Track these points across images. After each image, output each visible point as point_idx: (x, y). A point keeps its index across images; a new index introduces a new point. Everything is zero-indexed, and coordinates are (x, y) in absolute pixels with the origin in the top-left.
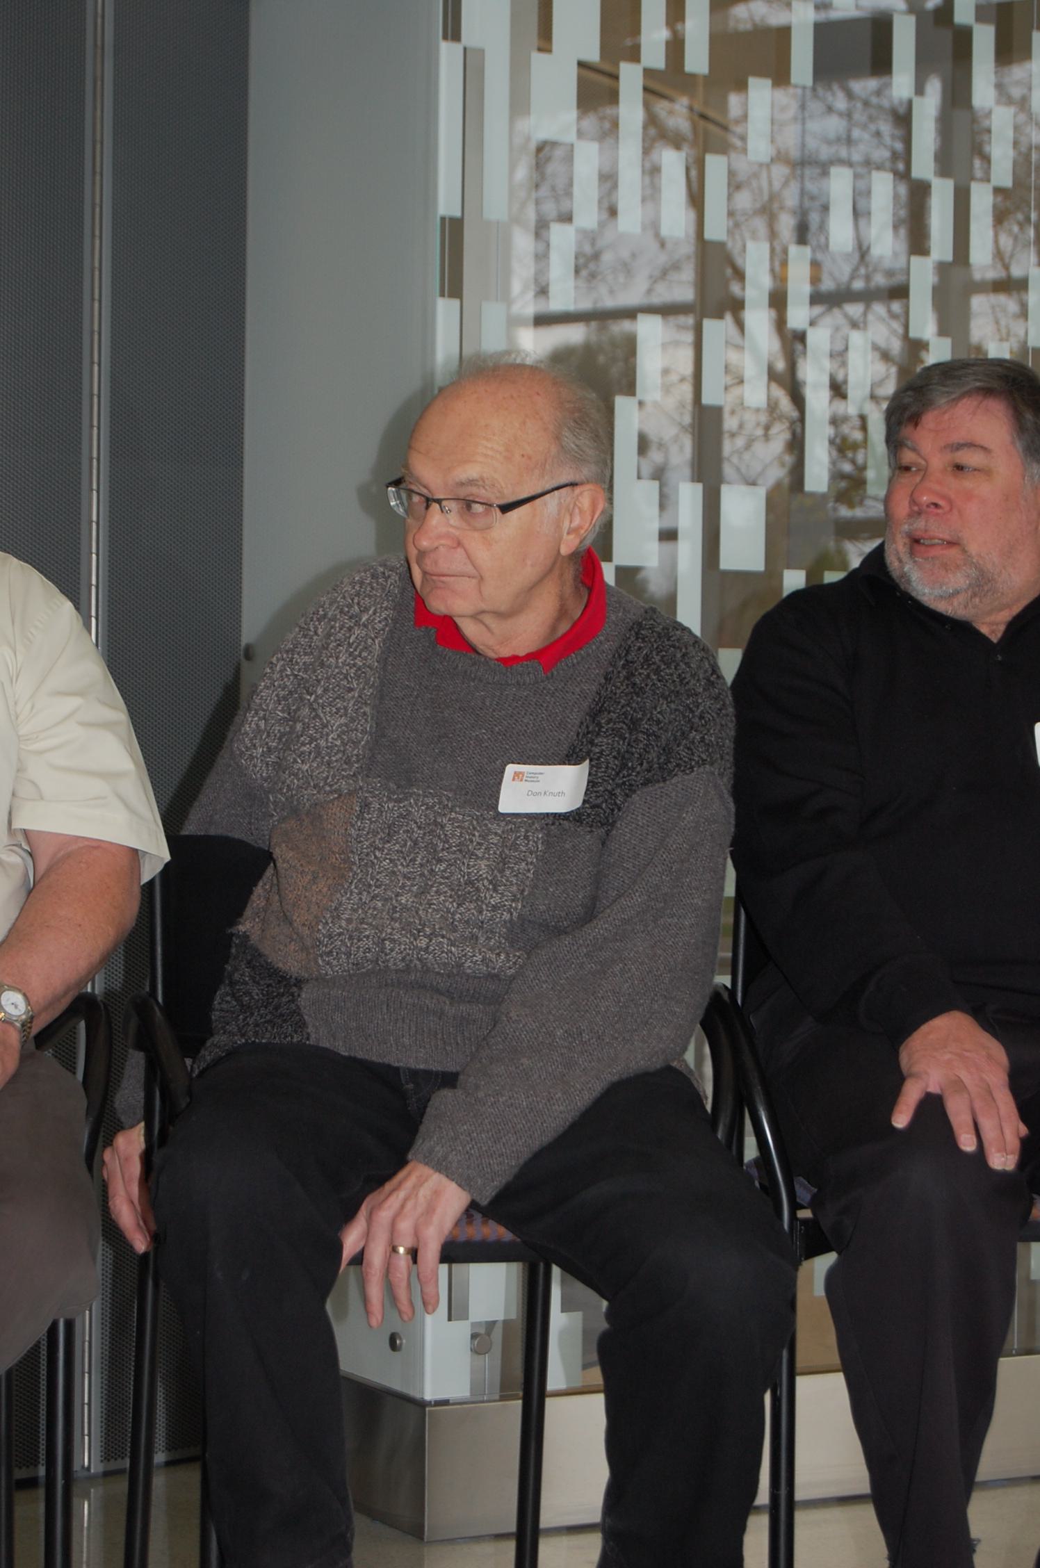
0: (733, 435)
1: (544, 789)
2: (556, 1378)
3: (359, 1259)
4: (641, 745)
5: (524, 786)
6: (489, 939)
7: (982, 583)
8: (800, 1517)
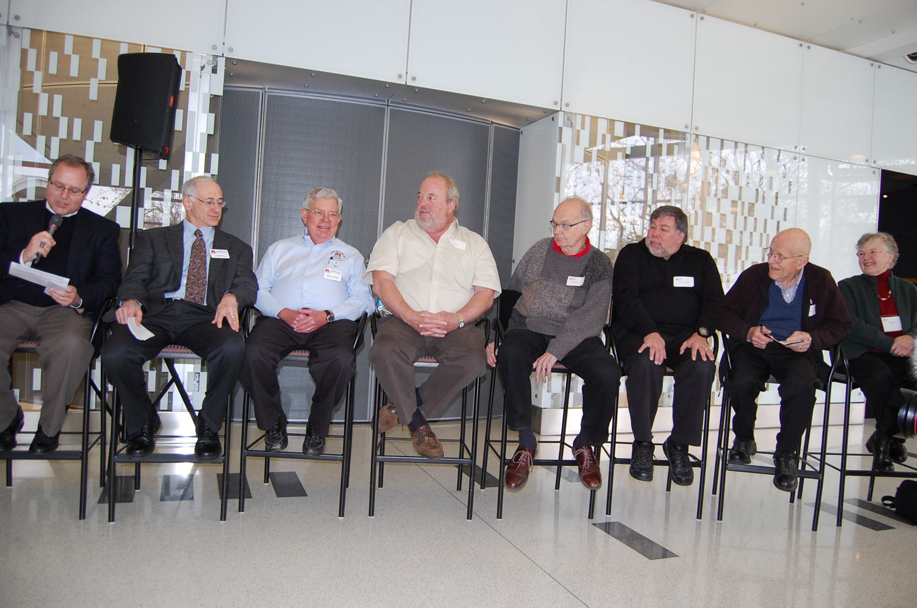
1: (576, 281)
2: (570, 404)
3: (535, 370)
7: (665, 252)
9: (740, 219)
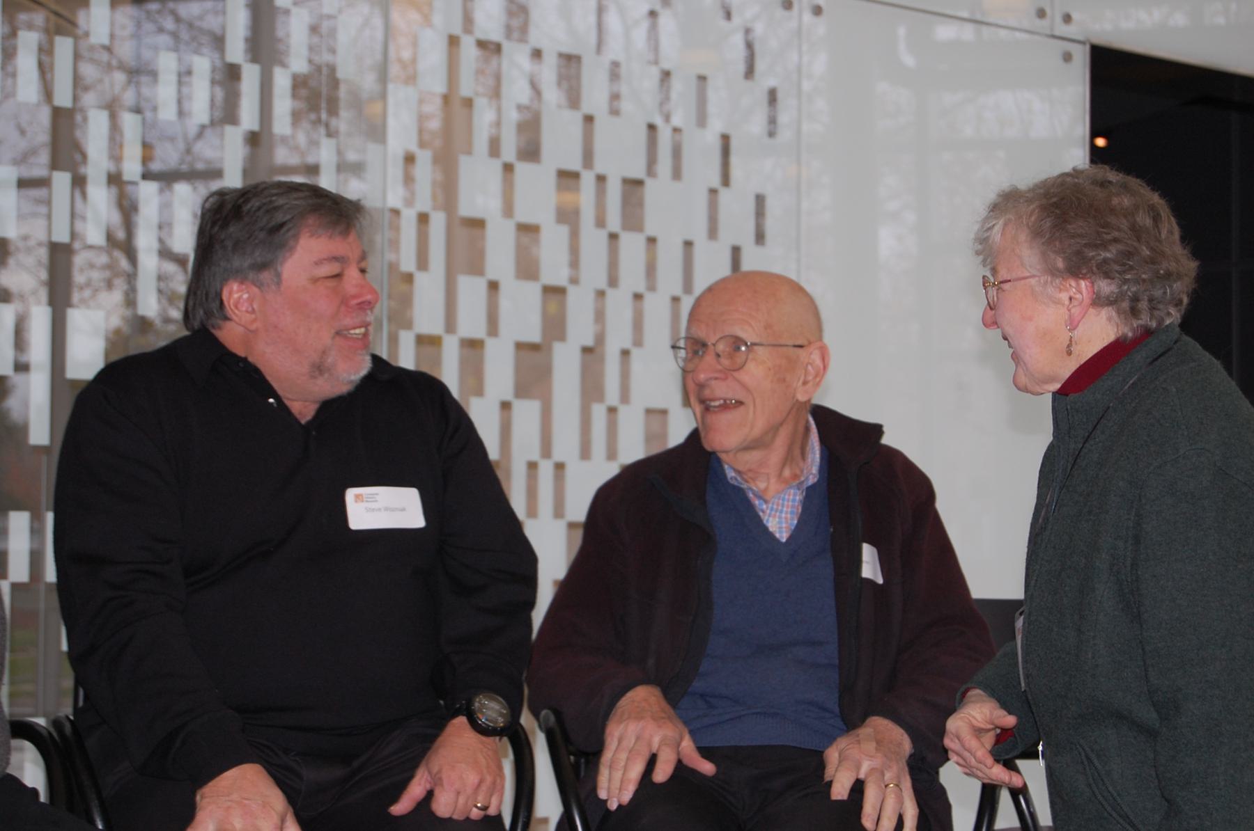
0: (81, 288)
9: (593, 242)
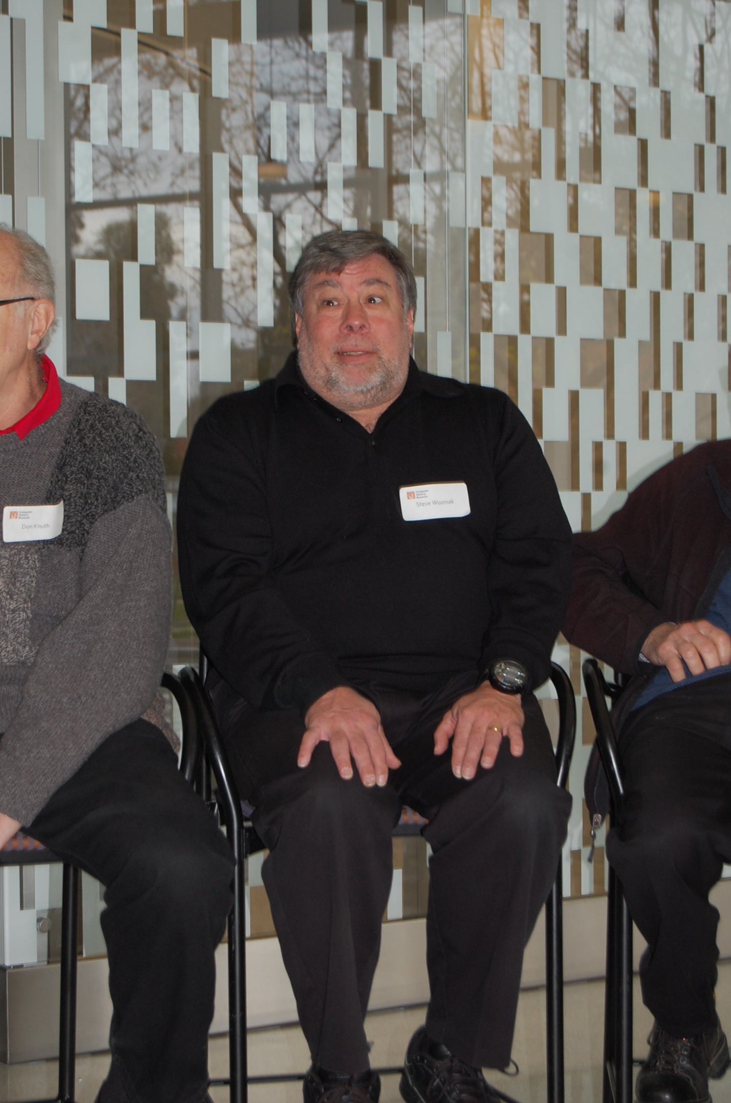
4: (95, 487)
5: (18, 522)
6: (17, 637)
8: (251, 1039)
9: (649, 252)
